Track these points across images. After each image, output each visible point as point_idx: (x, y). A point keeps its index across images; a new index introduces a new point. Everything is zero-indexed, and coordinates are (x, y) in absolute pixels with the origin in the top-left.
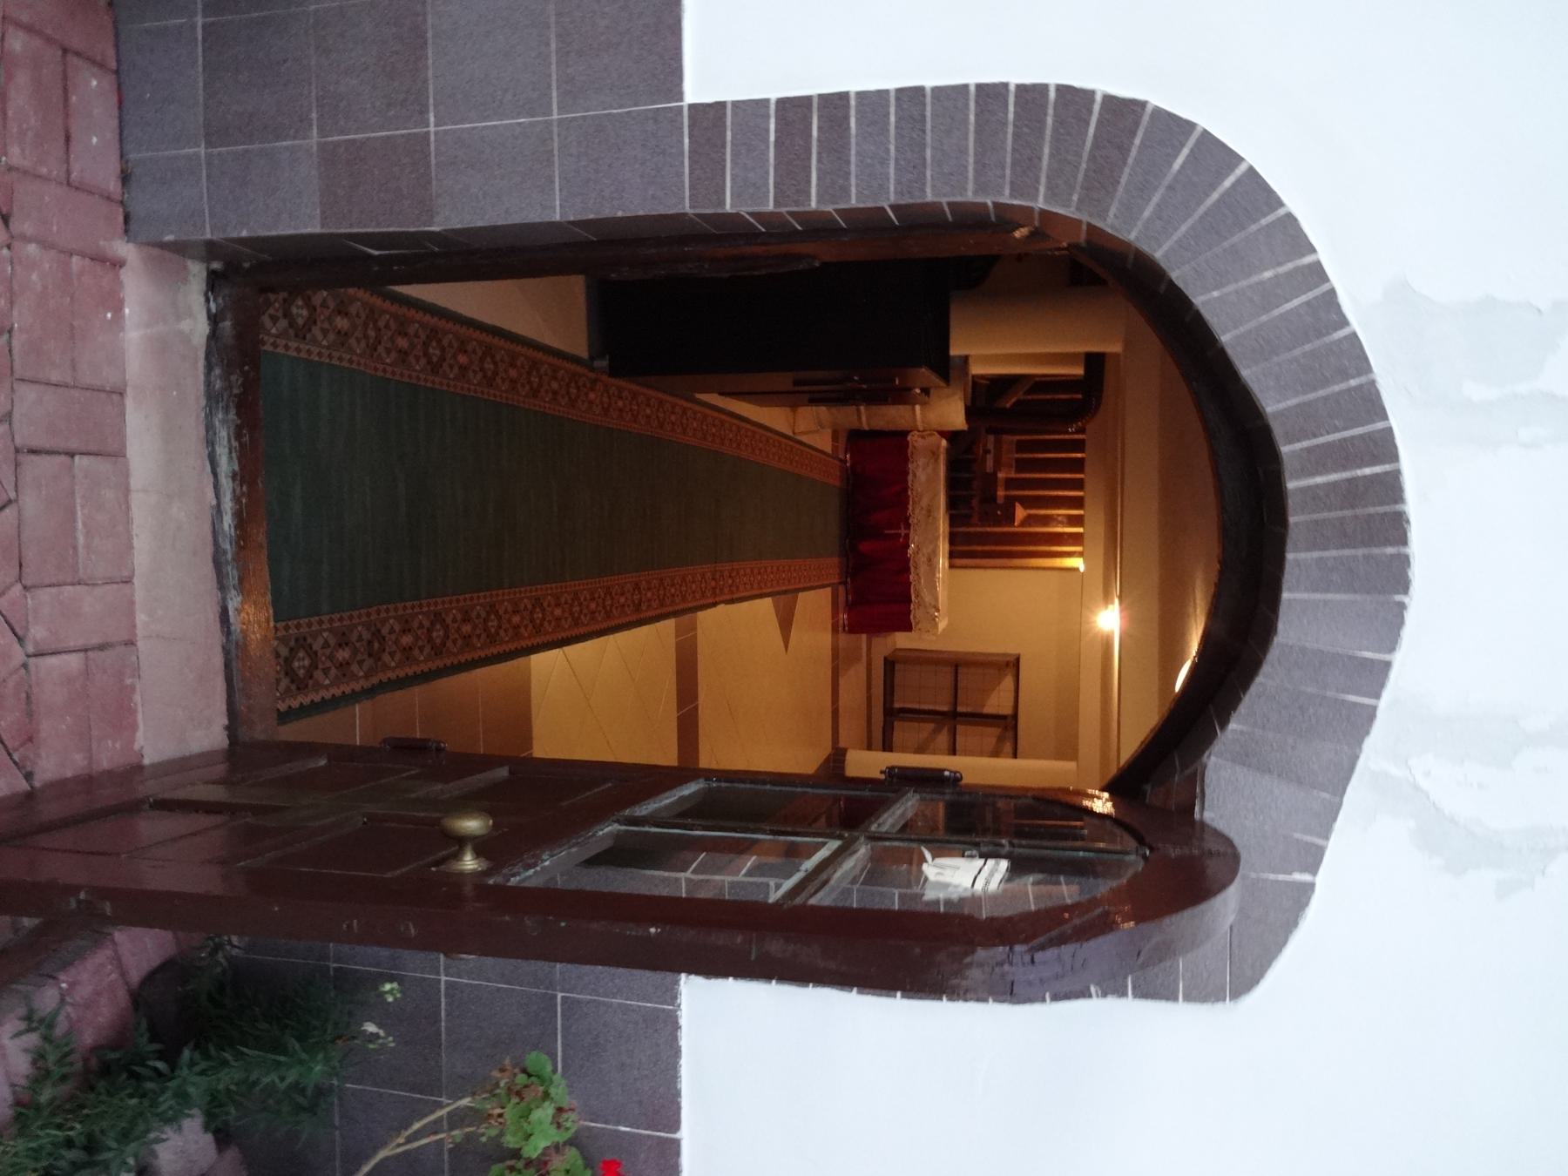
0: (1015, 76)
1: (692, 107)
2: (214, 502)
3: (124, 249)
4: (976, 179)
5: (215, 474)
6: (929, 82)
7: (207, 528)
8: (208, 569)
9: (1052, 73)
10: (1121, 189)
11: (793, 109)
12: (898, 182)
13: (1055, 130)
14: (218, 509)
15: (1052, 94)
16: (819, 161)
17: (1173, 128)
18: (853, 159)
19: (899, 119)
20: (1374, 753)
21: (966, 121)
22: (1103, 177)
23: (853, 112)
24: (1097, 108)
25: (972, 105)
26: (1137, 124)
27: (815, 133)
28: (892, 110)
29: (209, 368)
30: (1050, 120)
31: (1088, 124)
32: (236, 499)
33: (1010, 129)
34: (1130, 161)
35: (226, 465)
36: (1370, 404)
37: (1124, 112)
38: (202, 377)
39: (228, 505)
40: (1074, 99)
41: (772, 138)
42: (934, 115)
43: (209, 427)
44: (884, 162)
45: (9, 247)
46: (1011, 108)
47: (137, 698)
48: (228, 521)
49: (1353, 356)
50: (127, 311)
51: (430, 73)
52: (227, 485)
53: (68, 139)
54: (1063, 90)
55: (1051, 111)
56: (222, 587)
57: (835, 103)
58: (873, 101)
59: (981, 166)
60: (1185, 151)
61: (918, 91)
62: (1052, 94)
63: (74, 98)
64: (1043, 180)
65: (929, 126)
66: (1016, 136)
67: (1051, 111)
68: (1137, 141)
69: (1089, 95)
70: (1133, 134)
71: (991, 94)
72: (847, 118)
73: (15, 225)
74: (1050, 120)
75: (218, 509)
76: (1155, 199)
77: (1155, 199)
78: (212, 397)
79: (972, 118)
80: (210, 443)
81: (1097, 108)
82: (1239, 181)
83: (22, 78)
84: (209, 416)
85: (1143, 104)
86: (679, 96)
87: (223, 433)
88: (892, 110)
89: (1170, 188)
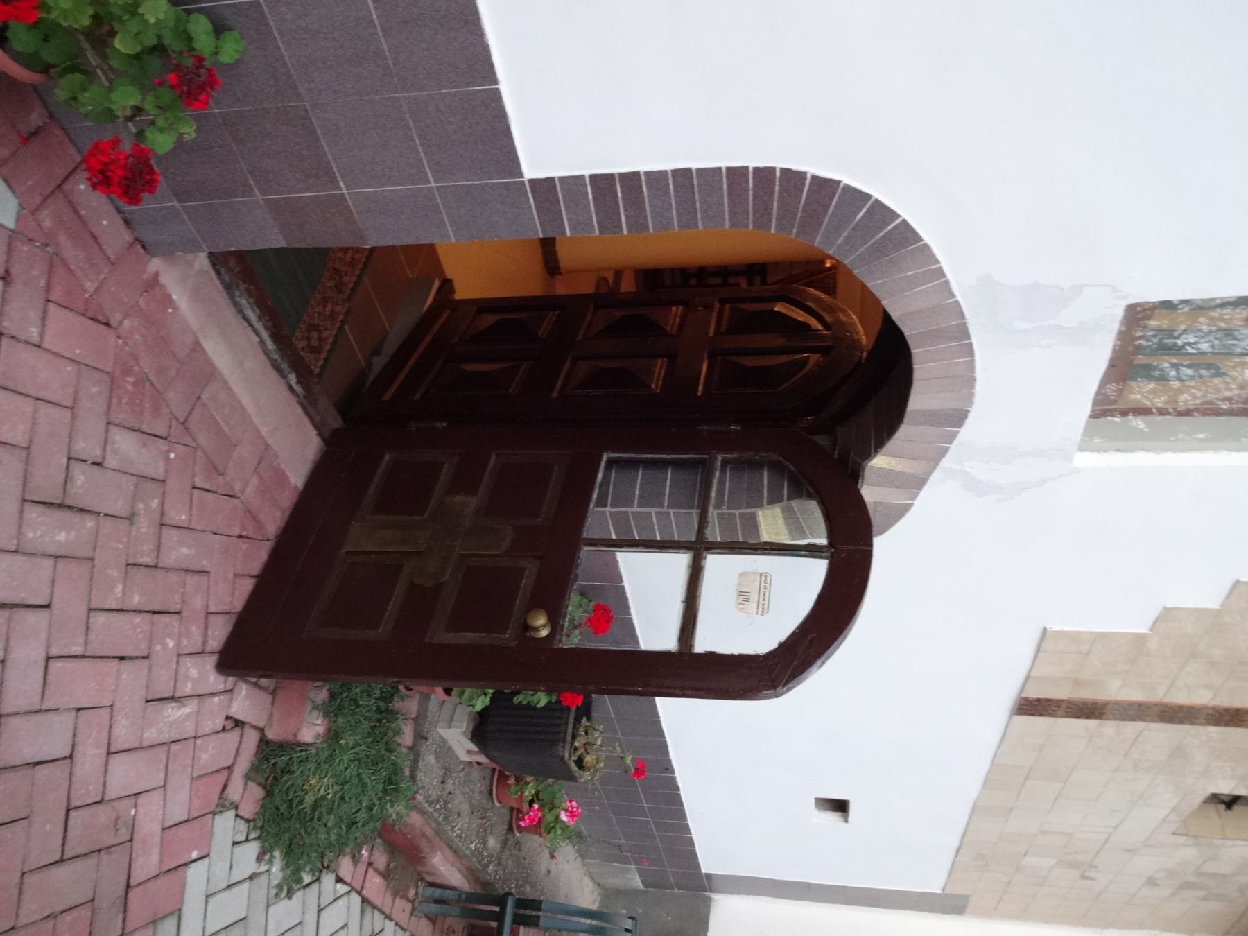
0: (753, 161)
1: (531, 181)
2: (258, 340)
3: (155, 265)
4: (730, 219)
5: (250, 325)
6: (694, 165)
7: (263, 357)
8: (274, 375)
9: (779, 161)
10: (823, 227)
11: (602, 182)
12: (679, 221)
13: (780, 193)
14: (262, 342)
15: (778, 174)
16: (625, 210)
18: (648, 209)
19: (675, 187)
21: (721, 188)
22: (812, 219)
23: (644, 183)
24: (808, 182)
25: (725, 179)
26: (834, 193)
27: (619, 194)
28: (671, 181)
29: (218, 273)
30: (777, 188)
31: (802, 191)
32: (267, 328)
33: (751, 192)
34: (829, 213)
35: (252, 315)
37: (825, 187)
38: (217, 282)
39: (265, 335)
40: (793, 178)
41: (591, 197)
42: (700, 186)
43: (236, 304)
44: (669, 209)
45: (119, 337)
46: (751, 181)
47: (282, 466)
48: (270, 344)
50: (174, 297)
51: (330, 157)
52: (259, 326)
53: (95, 238)
54: (785, 171)
55: (777, 183)
56: (284, 377)
57: (631, 179)
58: (656, 178)
59: (733, 214)
60: (864, 210)
61: (688, 171)
62: (778, 174)
63: (83, 212)
64: (774, 220)
65: (696, 190)
66: (755, 197)
67: (777, 183)
68: (834, 203)
69: (802, 175)
70: (831, 199)
71: (736, 174)
72: (641, 187)
73: (113, 323)
74: (777, 188)
75: (262, 342)
76: (845, 234)
77: (845, 234)
78: (228, 287)
79: (725, 186)
80: (241, 312)
81: (808, 182)
82: (896, 227)
83: (62, 238)
84: (232, 297)
85: (838, 182)
86: (521, 175)
87: (243, 302)
88: (671, 181)
89: (854, 229)
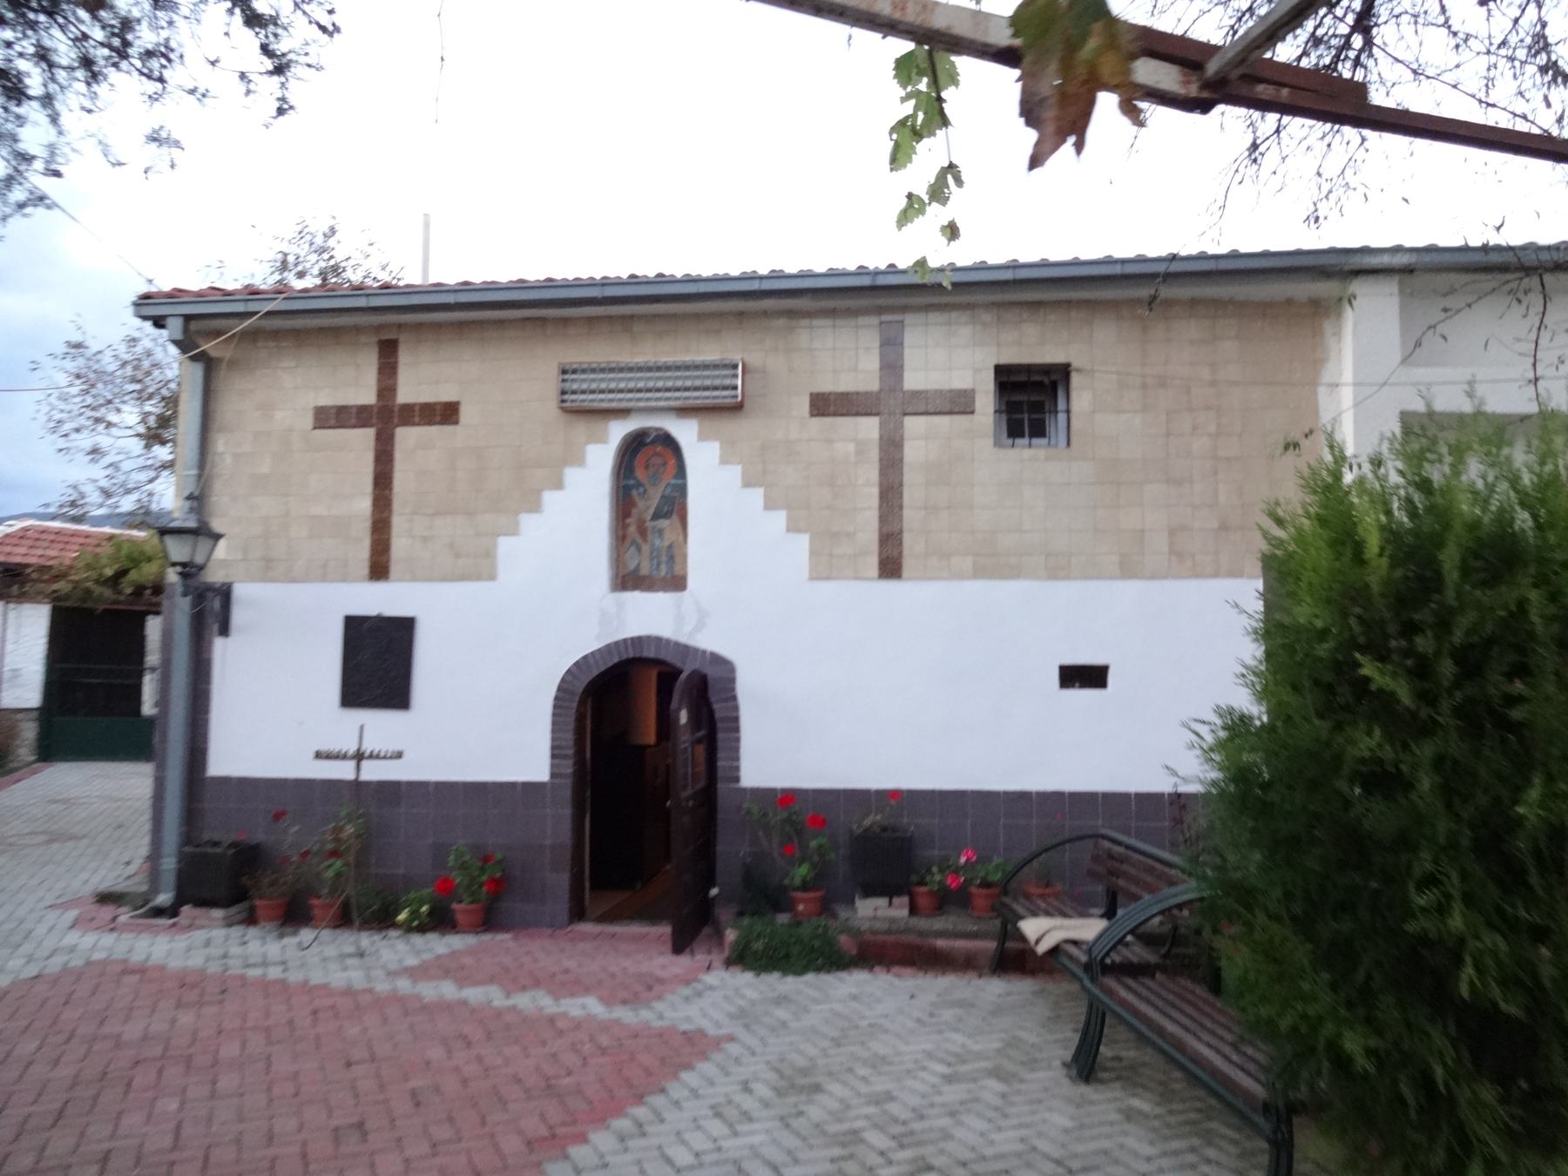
17: (563, 680)
20: (683, 640)
36: (617, 643)
49: (608, 646)
